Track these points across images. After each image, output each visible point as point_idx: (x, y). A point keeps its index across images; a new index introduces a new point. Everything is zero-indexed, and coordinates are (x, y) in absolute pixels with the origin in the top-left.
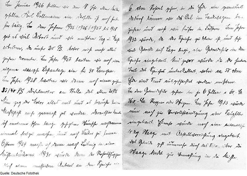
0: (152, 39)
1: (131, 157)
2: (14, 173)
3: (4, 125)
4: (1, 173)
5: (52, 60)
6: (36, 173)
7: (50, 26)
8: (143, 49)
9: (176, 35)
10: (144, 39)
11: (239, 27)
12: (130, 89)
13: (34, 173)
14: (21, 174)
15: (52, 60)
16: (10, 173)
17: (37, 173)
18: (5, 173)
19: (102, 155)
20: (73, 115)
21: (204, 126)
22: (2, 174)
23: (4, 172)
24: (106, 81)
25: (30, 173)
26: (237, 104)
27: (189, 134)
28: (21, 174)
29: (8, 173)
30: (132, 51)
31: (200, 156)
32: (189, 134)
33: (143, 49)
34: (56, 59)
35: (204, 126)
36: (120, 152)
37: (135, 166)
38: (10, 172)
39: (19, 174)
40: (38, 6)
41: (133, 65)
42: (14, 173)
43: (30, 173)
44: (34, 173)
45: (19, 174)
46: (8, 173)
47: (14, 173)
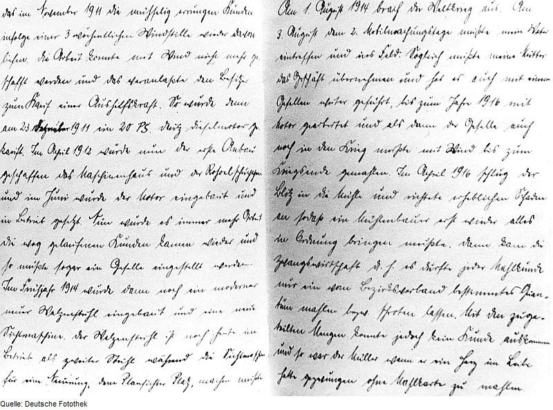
2: (32, 404)
3: (52, 288)
4: (3, 404)
6: (82, 403)
7: (452, 100)
9: (52, 48)
13: (75, 404)
14: (47, 404)
16: (23, 404)
18: (12, 404)
19: (215, 174)
20: (207, 37)
22: (5, 405)
23: (8, 401)
25: (67, 404)
28: (47, 404)
29: (18, 404)
30: (359, 150)
34: (232, 331)
36: (266, 350)
37: (285, 393)
38: (22, 400)
41: (287, 136)
42: (32, 403)
43: (67, 404)
44: (75, 404)
46: (18, 404)
47: (32, 404)
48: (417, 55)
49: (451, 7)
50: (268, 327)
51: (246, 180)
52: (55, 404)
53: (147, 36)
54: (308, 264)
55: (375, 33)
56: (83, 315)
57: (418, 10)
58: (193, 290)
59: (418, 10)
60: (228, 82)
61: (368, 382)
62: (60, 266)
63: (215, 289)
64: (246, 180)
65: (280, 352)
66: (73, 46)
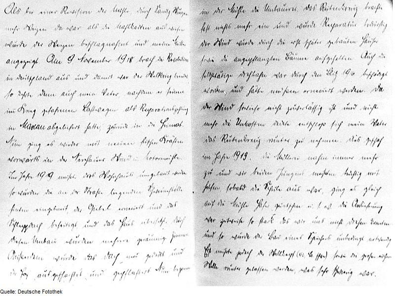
2: (23, 292)
4: (2, 291)
6: (58, 291)
13: (54, 291)
14: (33, 292)
16: (17, 292)
17: (60, 292)
18: (8, 291)
22: (3, 292)
23: (6, 289)
25: (48, 292)
28: (33, 292)
29: (13, 292)
42: (23, 291)
43: (48, 292)
44: (54, 291)
46: (13, 292)
47: (23, 292)
49: (130, 26)
50: (194, 237)
52: (39, 291)
53: (219, 45)
55: (318, 124)
58: (301, 124)
59: (61, 28)
60: (252, 111)
63: (299, 125)
65: (206, 235)
66: (294, 84)
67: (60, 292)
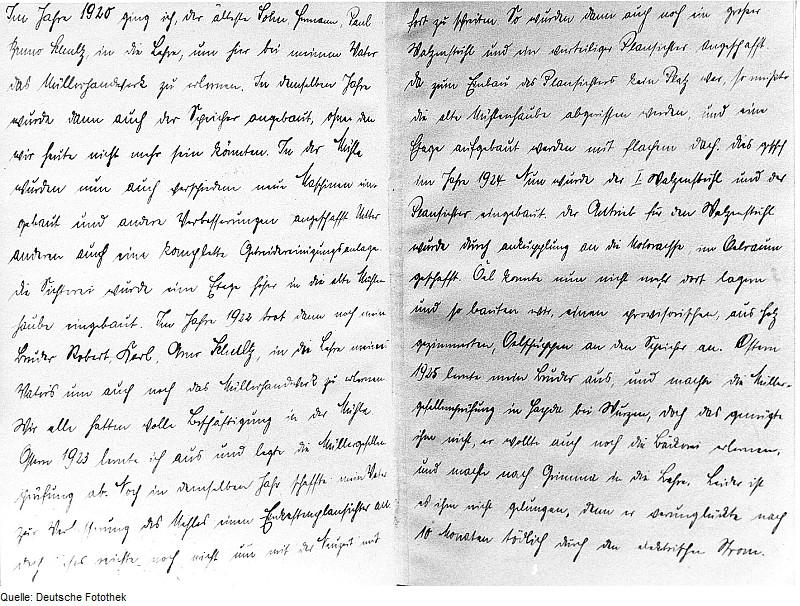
0: (443, 245)
1: (423, 547)
2: (46, 598)
4: (4, 597)
5: (193, 321)
6: (118, 597)
8: (253, 250)
10: (427, 244)
11: (455, 175)
12: (10, 9)
13: (109, 597)
14: (68, 598)
15: (193, 321)
16: (34, 598)
17: (121, 598)
18: (17, 597)
21: (610, 447)
22: (7, 598)
23: (12, 592)
24: (268, 187)
25: (98, 597)
26: (429, 248)
27: (314, 82)
28: (68, 598)
29: (26, 598)
31: (492, 409)
32: (314, 82)
33: (253, 250)
35: (610, 447)
36: (388, 434)
39: (61, 598)
40: (489, 182)
42: (46, 597)
43: (98, 597)
44: (109, 597)
45: (61, 598)
46: (26, 598)
47: (46, 598)
48: (266, 17)
50: (449, 587)
51: (540, 355)
54: (152, 155)
56: (458, 52)
57: (306, 350)
61: (460, 310)
62: (477, 114)
64: (540, 355)
67: (121, 598)
